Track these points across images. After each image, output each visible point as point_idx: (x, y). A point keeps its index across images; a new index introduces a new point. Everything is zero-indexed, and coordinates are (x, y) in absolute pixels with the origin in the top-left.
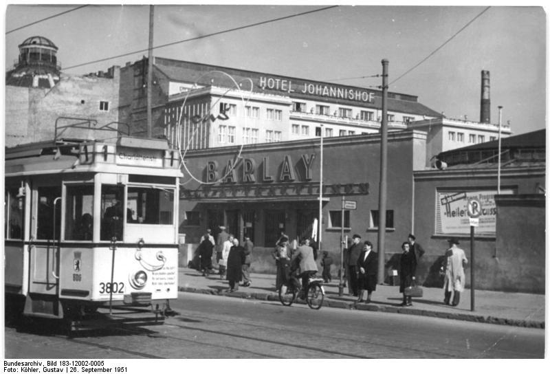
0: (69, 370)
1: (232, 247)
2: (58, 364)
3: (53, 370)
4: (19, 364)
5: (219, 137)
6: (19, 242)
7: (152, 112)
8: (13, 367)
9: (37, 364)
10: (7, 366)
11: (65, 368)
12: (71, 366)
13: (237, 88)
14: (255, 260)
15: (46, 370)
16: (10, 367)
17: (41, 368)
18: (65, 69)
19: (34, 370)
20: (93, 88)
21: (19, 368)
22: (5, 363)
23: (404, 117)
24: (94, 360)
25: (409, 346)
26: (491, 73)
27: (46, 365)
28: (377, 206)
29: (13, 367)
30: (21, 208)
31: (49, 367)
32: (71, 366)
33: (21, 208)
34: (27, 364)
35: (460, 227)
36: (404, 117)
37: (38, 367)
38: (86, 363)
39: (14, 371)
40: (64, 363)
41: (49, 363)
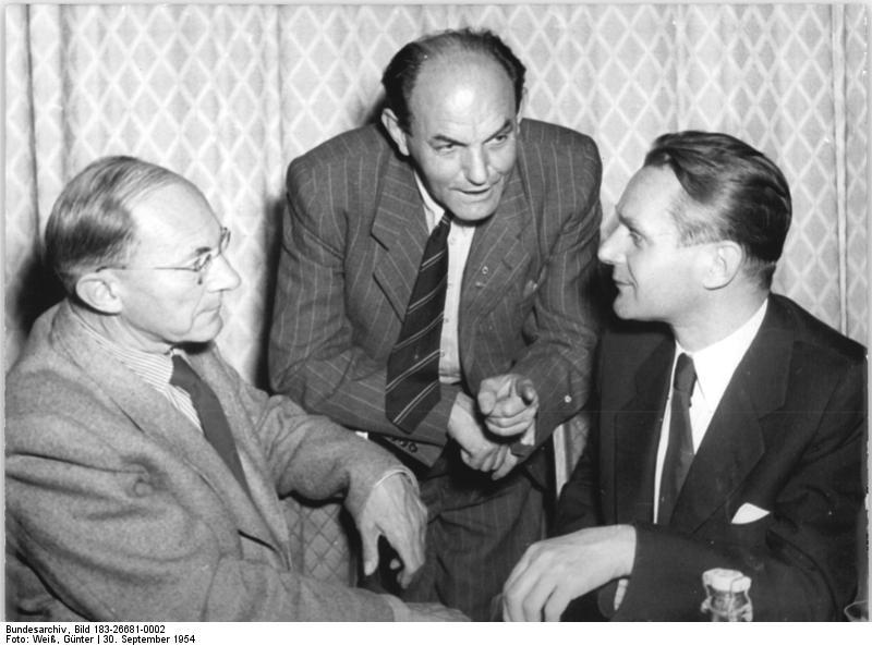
0: (102, 639)
4: (30, 630)
8: (21, 635)
10: (11, 633)
15: (68, 640)
16: (15, 635)
22: (8, 629)
24: (149, 624)
29: (21, 635)
34: (43, 630)
39: (23, 640)
41: (77, 629)
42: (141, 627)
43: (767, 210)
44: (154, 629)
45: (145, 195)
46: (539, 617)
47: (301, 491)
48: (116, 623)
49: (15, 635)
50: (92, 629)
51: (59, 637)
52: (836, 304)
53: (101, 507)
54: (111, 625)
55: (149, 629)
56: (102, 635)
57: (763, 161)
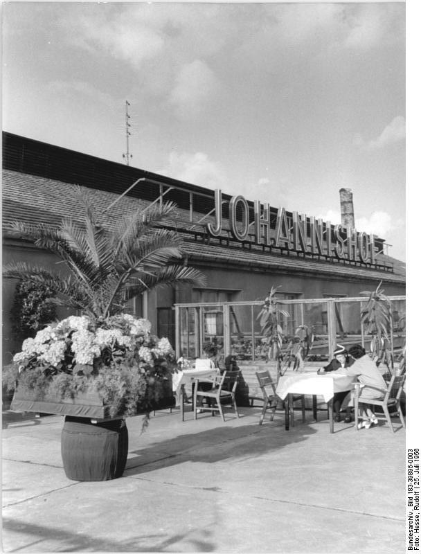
0: (417, 486)
1: (175, 403)
3: (417, 500)
4: (411, 535)
8: (414, 541)
9: (411, 517)
10: (413, 547)
11: (415, 490)
12: (413, 483)
13: (214, 211)
14: (217, 365)
15: (416, 508)
16: (414, 544)
17: (415, 513)
19: (417, 527)
20: (73, 351)
21: (415, 536)
22: (410, 549)
25: (319, 355)
26: (345, 187)
27: (413, 508)
29: (414, 541)
30: (361, 293)
31: (414, 503)
32: (414, 455)
33: (361, 293)
34: (411, 527)
37: (414, 515)
39: (418, 539)
41: (410, 505)
49: (414, 544)
50: (411, 495)
55: (410, 460)
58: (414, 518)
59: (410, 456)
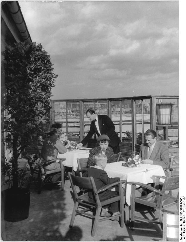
0: (184, 212)
2: (181, 216)
3: (184, 218)
4: (182, 234)
5: (46, 174)
6: (177, 127)
7: (159, 125)
8: (183, 236)
9: (182, 226)
10: (183, 239)
11: (183, 214)
12: (182, 211)
15: (184, 222)
16: (183, 238)
17: (183, 224)
18: (166, 122)
19: (184, 230)
21: (183, 234)
22: (181, 240)
23: (6, 150)
24: (180, 201)
27: (182, 222)
28: (177, 120)
29: (183, 236)
31: (183, 220)
34: (182, 230)
35: (70, 179)
36: (6, 150)
37: (183, 225)
38: (181, 213)
39: (185, 236)
40: (181, 214)
41: (181, 221)
42: (181, 203)
43: (163, 202)
44: (181, 199)
45: (133, 200)
46: (178, 148)
47: (120, 203)
48: (180, 210)
49: (183, 238)
51: (183, 224)
52: (160, 221)
53: (157, 98)
54: (180, 211)
55: (181, 201)
56: (183, 212)
57: (83, 128)
58: (183, 226)
59: (181, 199)
